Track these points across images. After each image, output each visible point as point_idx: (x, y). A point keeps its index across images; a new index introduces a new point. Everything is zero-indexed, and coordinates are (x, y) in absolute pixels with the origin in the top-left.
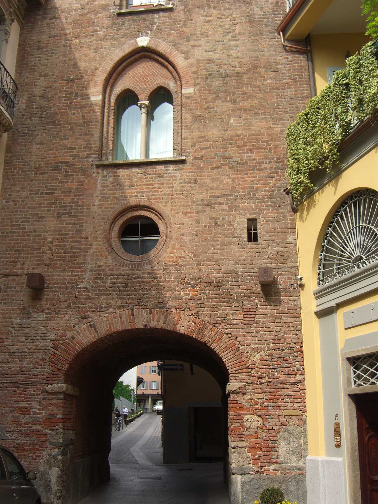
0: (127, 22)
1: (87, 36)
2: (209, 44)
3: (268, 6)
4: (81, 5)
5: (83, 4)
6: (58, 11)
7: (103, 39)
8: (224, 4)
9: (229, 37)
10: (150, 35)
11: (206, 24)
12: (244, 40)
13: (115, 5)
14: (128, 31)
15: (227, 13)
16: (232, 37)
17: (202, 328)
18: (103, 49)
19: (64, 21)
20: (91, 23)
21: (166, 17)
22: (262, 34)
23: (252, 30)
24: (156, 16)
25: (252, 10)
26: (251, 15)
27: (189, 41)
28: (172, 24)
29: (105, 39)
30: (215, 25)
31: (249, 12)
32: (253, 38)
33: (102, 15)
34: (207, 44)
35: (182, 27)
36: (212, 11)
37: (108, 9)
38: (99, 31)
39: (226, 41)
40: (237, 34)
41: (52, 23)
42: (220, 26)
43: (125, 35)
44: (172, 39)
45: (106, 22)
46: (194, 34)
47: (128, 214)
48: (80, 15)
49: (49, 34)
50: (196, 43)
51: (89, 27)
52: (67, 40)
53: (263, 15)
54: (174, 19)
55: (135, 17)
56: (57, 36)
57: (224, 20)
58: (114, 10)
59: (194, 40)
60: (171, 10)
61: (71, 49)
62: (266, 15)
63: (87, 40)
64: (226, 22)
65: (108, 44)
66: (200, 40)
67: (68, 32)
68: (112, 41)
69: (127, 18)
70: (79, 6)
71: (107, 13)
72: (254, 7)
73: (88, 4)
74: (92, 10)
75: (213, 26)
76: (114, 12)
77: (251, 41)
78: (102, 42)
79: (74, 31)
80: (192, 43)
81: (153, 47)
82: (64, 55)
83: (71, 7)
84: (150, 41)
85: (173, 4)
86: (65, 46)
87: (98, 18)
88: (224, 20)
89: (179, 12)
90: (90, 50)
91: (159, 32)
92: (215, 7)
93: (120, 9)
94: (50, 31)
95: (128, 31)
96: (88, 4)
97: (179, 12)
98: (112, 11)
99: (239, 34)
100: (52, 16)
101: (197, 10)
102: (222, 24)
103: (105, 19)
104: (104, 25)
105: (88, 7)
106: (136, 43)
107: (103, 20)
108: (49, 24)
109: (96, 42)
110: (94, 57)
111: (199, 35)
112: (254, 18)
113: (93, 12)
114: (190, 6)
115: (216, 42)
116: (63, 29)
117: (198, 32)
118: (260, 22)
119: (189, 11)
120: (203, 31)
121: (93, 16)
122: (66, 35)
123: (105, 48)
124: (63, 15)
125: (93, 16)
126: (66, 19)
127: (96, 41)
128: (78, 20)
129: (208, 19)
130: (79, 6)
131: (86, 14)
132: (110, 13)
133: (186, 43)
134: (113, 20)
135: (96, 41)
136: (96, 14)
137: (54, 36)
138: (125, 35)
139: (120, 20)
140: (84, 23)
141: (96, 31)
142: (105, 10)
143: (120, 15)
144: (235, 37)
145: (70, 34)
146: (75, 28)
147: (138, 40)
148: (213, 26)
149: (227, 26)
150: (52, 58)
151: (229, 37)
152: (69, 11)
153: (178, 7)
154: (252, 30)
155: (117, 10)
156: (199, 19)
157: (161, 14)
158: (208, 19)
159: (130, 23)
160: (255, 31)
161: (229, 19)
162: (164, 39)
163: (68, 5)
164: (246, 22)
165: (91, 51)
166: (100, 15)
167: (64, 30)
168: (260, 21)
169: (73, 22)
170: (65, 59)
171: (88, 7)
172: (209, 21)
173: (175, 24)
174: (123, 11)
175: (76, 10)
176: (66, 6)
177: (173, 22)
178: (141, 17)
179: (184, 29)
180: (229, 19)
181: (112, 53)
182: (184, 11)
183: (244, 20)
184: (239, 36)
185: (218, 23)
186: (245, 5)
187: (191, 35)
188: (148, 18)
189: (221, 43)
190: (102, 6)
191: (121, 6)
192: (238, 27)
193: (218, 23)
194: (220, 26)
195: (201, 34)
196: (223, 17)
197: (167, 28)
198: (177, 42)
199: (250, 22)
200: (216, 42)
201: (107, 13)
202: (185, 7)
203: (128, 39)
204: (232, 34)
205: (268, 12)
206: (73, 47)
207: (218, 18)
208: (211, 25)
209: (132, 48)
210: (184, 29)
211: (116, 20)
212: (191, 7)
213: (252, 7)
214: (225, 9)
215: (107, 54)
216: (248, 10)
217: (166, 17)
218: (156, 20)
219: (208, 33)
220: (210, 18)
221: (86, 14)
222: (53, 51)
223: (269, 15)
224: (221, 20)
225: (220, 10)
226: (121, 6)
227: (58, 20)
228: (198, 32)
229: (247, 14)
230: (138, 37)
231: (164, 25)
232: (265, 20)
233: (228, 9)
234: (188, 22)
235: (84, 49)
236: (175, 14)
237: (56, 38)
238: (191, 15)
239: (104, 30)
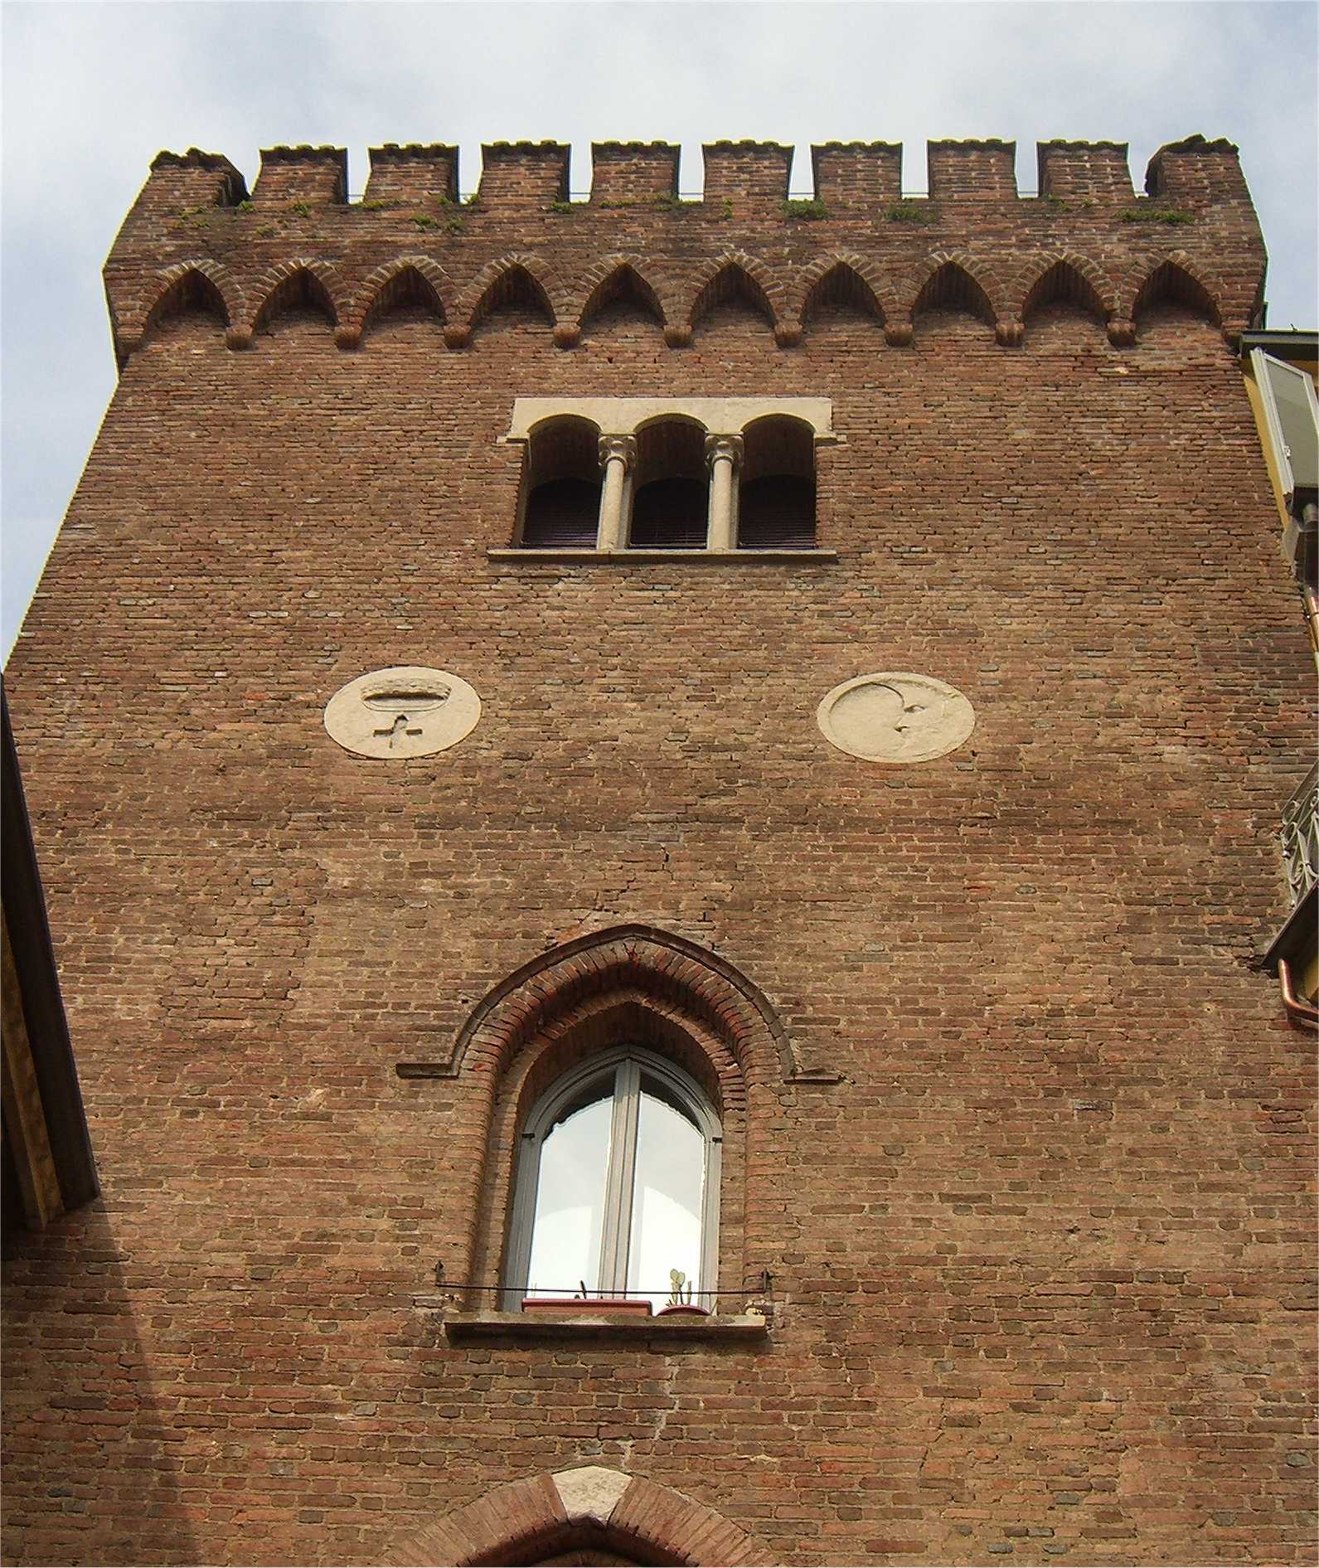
0: (506, 1378)
1: (269, 1426)
2: (968, 1542)
3: (1289, 1371)
4: (251, 1260)
5: (266, 1260)
6: (117, 1272)
7: (360, 1457)
8: (1043, 1340)
9: (1081, 1515)
10: (634, 1463)
11: (950, 1432)
12: (1167, 1537)
13: (440, 1285)
14: (504, 1429)
15: (1066, 1385)
16: (1101, 1517)
17: (86, 809)
18: (358, 1508)
19: (145, 1329)
20: (294, 1363)
21: (726, 1375)
22: (1264, 1515)
23: (1210, 1486)
24: (669, 1365)
25: (1204, 1382)
26: (1197, 1410)
27: (856, 1515)
28: (758, 1419)
29: (370, 1455)
30: (1003, 1445)
31: (1186, 1393)
32: (1217, 1531)
33: (364, 1326)
34: (956, 1543)
35: (817, 1436)
36: (980, 1367)
37: (398, 1300)
38: (343, 1410)
39: (1065, 1535)
40: (1127, 1505)
41: (77, 1334)
42: (1032, 1454)
43: (486, 1449)
44: (759, 1494)
45: (385, 1363)
46: (885, 1483)
47: (49, 1166)
48: (241, 1312)
49: (53, 1387)
50: (895, 1531)
51: (288, 1378)
52: (152, 1434)
53: (1264, 1412)
54: (771, 1391)
55: (550, 1359)
56: (99, 1404)
57: (1045, 1421)
58: (435, 1307)
59: (884, 1514)
60: (753, 1340)
61: (169, 1482)
62: (1283, 1412)
63: (271, 1448)
64: (1067, 1435)
65: (388, 1482)
66: (917, 1515)
67: (162, 1389)
68: (408, 1470)
69: (504, 1357)
70: (237, 1263)
71: (393, 1319)
72: (1212, 1366)
73: (288, 1260)
74: (313, 1291)
75: (989, 1451)
76: (432, 1318)
77: (1210, 1547)
78: (356, 1468)
79: (196, 1388)
80: (871, 1527)
81: (651, 1528)
82: (128, 1511)
83: (196, 1264)
84: (628, 1495)
85: (766, 1311)
86: (137, 1462)
87: (344, 1339)
88: (1045, 1421)
89: (797, 1358)
90: (281, 1502)
91: (679, 1454)
92: (994, 1352)
93: (468, 1306)
94: (60, 1374)
95: (504, 1429)
96: (288, 1260)
97: (797, 1358)
98: (421, 1312)
99: (1141, 1501)
100: (79, 1295)
101: (896, 1355)
102: (1043, 1440)
103: (380, 1351)
104: (374, 1380)
105: (290, 1274)
106: (553, 1494)
107: (369, 1356)
108: (63, 1334)
109: (320, 1467)
110: (299, 1544)
111: (914, 1491)
112: (1216, 1427)
113: (317, 1304)
114: (857, 1334)
115: (1009, 1533)
116: (135, 1372)
117: (909, 1475)
118: (1249, 1447)
119: (855, 1359)
120: (936, 1467)
121: (312, 1327)
122: (153, 1404)
123: (368, 1505)
124: (144, 1302)
125: (312, 1327)
126: (160, 1322)
127: (320, 1456)
128: (229, 1336)
129: (958, 1407)
130: (237, 1263)
131: (276, 1313)
132: (414, 1318)
133: (836, 1526)
134: (424, 1358)
135: (320, 1456)
136: (333, 1316)
137: (79, 1405)
138: (486, 1449)
139: (466, 1363)
140: (263, 1353)
141: (326, 1408)
142: (382, 1300)
143: (464, 1336)
144: (1116, 1516)
145: (171, 1406)
146: (203, 1377)
147: (564, 1480)
148: (989, 1451)
149: (1066, 1455)
150: (53, 1518)
151: (1081, 1515)
152: (179, 1281)
153: (790, 1333)
154: (1210, 1486)
155: (450, 1309)
156: (909, 1402)
157: (698, 1358)
158: (958, 1407)
159: (519, 1386)
160: (1229, 1490)
161: (1076, 1420)
162: (713, 1494)
163: (175, 1252)
164: (1172, 1444)
165: (285, 1513)
166: (352, 1325)
167: (144, 1376)
168: (1249, 1443)
169: (196, 1344)
170: (126, 1535)
171: (290, 1274)
172: (966, 1422)
173: (777, 1419)
174: (487, 1316)
175: (221, 1282)
176: (165, 1253)
177: (766, 1406)
178: (586, 1361)
179: (826, 1449)
180: (1076, 1420)
181: (407, 1535)
182: (823, 1352)
183: (1162, 1432)
184: (1135, 1510)
185: (1019, 1433)
186: (1161, 1355)
187: (864, 1483)
188: (620, 1372)
189: (1039, 1544)
190: (367, 1279)
191: (471, 1290)
192: (1128, 1464)
193: (1019, 1433)
194: (1032, 1454)
195: (925, 1484)
196: (1045, 1406)
197: (728, 1436)
198: (786, 1513)
199: (1189, 1441)
200: (1009, 1533)
201: (393, 1319)
202: (831, 1337)
203: (504, 1472)
204: (1094, 1497)
205: (1291, 1397)
206: (182, 1473)
207: (1017, 1408)
208: (982, 1440)
209: (523, 1523)
210: (826, 1449)
211: (437, 1359)
212: (867, 1336)
213: (1200, 1368)
214: (1053, 1367)
215: (378, 1537)
216: (1180, 1381)
217: (726, 1375)
218: (667, 1387)
219: (960, 1483)
220: (972, 1405)
221: (276, 1313)
222: (65, 1484)
223: (1300, 1413)
224: (1032, 1420)
225: (1025, 1366)
226: (471, 1290)
227: (117, 1323)
228: (909, 1475)
229: (1178, 1402)
230: (564, 1464)
231: (716, 1419)
232: (1280, 1440)
233: (1071, 1366)
234: (848, 1416)
235: (247, 1493)
236: (777, 1362)
237: (88, 1415)
238: (863, 1381)
239: (370, 1407)
